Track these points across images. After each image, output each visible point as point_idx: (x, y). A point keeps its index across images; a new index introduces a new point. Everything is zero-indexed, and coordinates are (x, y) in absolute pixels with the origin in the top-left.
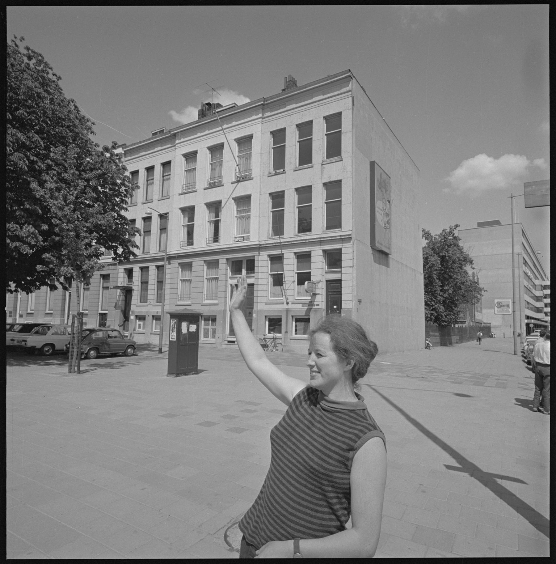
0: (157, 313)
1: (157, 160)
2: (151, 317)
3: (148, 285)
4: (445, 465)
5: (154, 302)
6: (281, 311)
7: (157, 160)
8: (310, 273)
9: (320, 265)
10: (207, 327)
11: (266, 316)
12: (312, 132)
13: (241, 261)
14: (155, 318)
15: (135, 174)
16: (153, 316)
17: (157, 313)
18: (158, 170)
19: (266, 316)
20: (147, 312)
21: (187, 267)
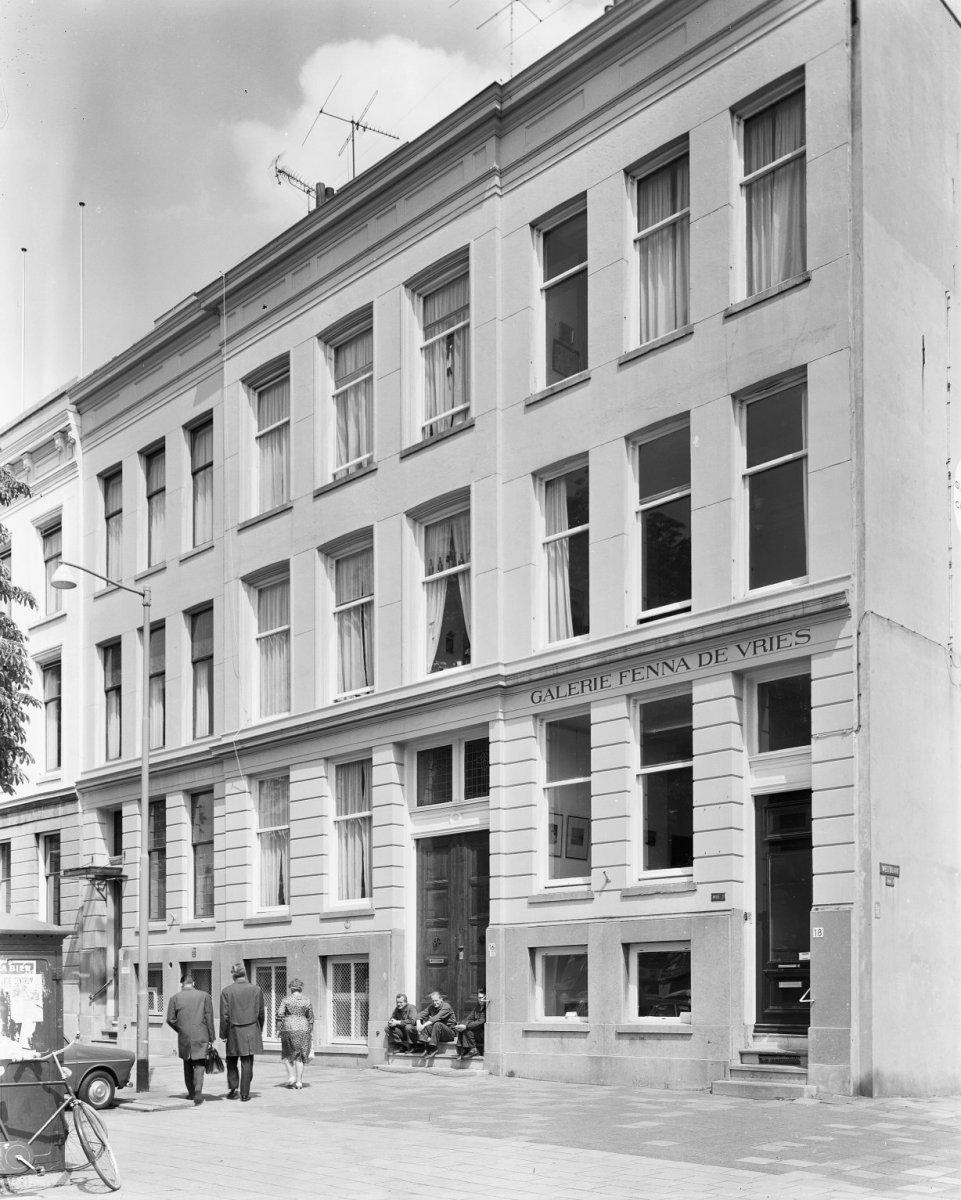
0: (194, 954)
1: (168, 420)
2: (177, 971)
3: (212, 851)
4: (283, 154)
5: (187, 917)
6: (582, 925)
7: (168, 420)
8: (690, 770)
9: (396, 794)
10: (342, 996)
11: (532, 951)
12: (688, 975)
13: (446, 752)
14: (189, 973)
15: (155, 498)
16: (184, 965)
17: (194, 954)
18: (179, 455)
19: (532, 951)
20: (165, 952)
21: (275, 784)
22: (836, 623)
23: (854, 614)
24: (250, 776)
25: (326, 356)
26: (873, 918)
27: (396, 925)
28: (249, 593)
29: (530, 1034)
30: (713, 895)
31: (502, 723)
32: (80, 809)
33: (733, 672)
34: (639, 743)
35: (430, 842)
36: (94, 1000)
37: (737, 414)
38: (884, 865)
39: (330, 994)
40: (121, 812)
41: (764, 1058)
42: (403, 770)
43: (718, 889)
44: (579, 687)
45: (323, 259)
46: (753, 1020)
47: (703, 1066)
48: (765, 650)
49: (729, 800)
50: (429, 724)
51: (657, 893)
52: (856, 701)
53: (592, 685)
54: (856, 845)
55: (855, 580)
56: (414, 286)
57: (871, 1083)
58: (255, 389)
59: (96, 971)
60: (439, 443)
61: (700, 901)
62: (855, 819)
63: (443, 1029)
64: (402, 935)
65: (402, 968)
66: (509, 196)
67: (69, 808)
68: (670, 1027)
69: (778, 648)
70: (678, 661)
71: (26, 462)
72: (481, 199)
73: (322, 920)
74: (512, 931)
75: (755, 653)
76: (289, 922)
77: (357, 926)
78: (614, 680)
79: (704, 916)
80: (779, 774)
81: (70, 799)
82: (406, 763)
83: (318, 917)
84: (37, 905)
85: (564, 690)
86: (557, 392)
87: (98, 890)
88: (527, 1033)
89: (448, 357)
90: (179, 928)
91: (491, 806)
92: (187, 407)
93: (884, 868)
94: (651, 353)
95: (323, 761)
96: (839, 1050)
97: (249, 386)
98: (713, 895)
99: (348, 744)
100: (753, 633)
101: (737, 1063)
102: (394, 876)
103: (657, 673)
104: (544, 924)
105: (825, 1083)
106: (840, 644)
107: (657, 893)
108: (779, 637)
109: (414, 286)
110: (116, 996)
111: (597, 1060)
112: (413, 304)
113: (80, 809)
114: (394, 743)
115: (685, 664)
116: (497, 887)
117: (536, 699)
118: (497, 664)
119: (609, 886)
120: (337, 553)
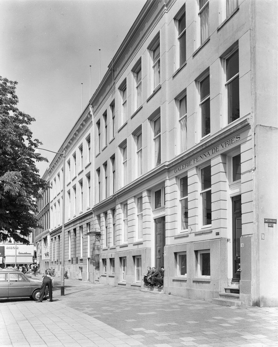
6: (185, 245)
9: (223, 177)
11: (176, 254)
19: (176, 254)
22: (247, 131)
23: (252, 127)
24: (135, 197)
25: (134, 76)
26: (260, 239)
27: (148, 246)
28: (121, 151)
29: (174, 281)
30: (216, 233)
31: (168, 181)
32: (93, 216)
33: (221, 154)
34: (200, 181)
35: (161, 219)
36: (96, 269)
37: (223, 63)
38: (266, 219)
39: (136, 267)
40: (107, 213)
41: (232, 291)
42: (150, 198)
43: (217, 231)
44: (184, 166)
45: (128, 54)
46: (232, 277)
47: (212, 293)
48: (228, 145)
49: (220, 199)
50: (140, 190)
51: (203, 233)
52: (254, 159)
53: (188, 165)
54: (254, 213)
55: (253, 115)
56: (150, 48)
57: (259, 302)
58: (122, 90)
59: (97, 261)
60: (179, 72)
61: (213, 236)
62: (254, 203)
63: (155, 279)
64: (150, 249)
65: (150, 259)
66: (169, 12)
67: (90, 217)
68: (205, 279)
69: (232, 143)
70: (207, 153)
71: (77, 133)
72: (162, 16)
73: (134, 245)
74: (170, 247)
75: (226, 146)
76: (127, 246)
77: (140, 246)
78: (192, 162)
79: (213, 240)
80: (236, 189)
81: (91, 214)
82: (151, 196)
83: (132, 244)
84: (87, 243)
85: (210, 152)
86: (156, 92)
87: (97, 238)
88: (173, 280)
89: (159, 68)
90: (102, 249)
91: (242, 182)
92: (109, 101)
93: (266, 221)
94: (200, 50)
95: (133, 197)
96: (248, 290)
97: (120, 90)
98: (216, 233)
99: (136, 192)
100: (213, 146)
101: (224, 292)
102: (222, 214)
103: (202, 158)
104: (177, 245)
105: (244, 301)
106: (248, 138)
107: (203, 233)
108: (232, 140)
109: (150, 48)
110: (141, 267)
111: (188, 290)
112: (150, 54)
113: (93, 216)
114: (146, 190)
115: (209, 154)
116: (168, 233)
117: (176, 172)
118: (166, 162)
119: (192, 232)
120: (124, 146)
